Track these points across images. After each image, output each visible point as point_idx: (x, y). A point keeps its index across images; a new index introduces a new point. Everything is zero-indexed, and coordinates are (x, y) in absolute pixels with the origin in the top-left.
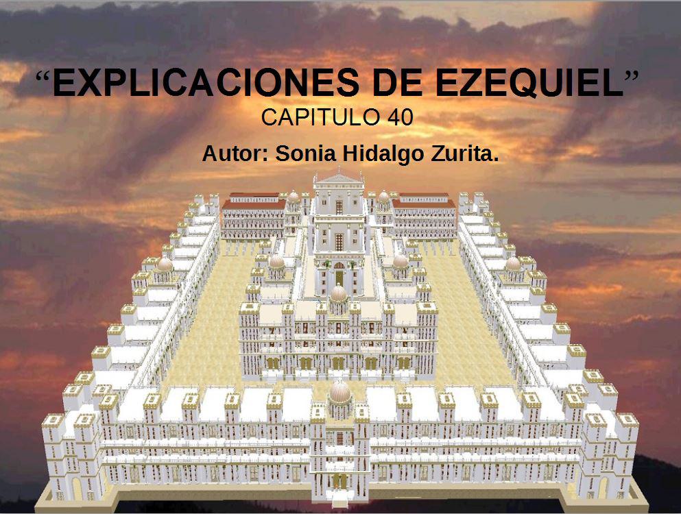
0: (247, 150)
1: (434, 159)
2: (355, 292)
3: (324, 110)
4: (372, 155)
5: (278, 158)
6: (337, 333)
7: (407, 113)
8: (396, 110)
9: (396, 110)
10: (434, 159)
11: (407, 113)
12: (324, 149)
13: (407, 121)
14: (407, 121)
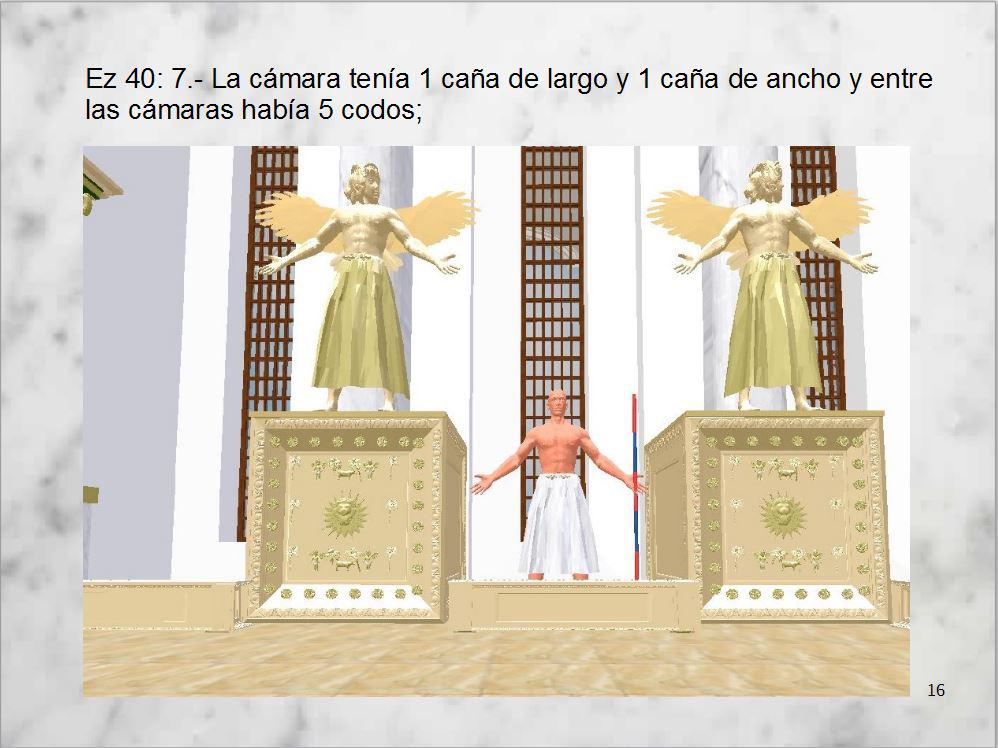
0: (512, 86)
1: (114, 75)
3: (89, 78)
4: (378, 111)
7: (148, 73)
8: (136, 70)
9: (136, 70)
10: (114, 75)
11: (148, 73)
13: (148, 83)
14: (148, 83)
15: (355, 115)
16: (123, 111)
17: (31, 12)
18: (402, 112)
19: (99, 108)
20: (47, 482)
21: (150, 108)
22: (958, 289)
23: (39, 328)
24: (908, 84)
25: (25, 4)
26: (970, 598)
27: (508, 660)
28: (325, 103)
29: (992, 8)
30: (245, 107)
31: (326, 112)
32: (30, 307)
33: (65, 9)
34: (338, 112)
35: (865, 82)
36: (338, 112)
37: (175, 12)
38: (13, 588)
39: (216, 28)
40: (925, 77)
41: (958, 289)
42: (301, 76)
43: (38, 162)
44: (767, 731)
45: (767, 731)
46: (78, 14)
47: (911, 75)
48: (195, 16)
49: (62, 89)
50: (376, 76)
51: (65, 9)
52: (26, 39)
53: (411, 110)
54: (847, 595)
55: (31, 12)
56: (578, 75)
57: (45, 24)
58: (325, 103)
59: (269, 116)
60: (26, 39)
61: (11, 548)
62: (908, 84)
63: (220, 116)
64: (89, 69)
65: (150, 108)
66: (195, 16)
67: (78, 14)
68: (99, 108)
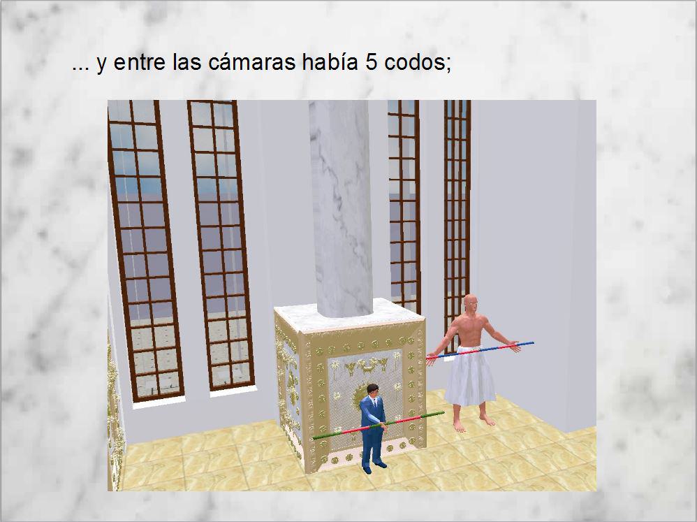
2: (43, 234)
5: (199, 60)
6: (469, 102)
12: (346, 57)
15: (396, 67)
16: (204, 62)
17: (22, 8)
18: (434, 64)
19: (184, 61)
20: (33, 336)
21: (226, 61)
22: (670, 201)
23: (28, 229)
24: (146, 66)
25: (17, 2)
26: (678, 417)
27: (174, 460)
28: (371, 57)
29: (694, 4)
30: (305, 60)
31: (372, 64)
32: (22, 214)
33: (47, 5)
34: (381, 64)
35: (110, 65)
36: (381, 64)
37: (123, 8)
38: (9, 410)
39: (152, 18)
40: (158, 61)
41: (670, 201)
42: (314, 60)
43: (27, 113)
44: (536, 510)
45: (536, 510)
46: (55, 9)
47: (149, 60)
48: (136, 11)
49: (43, 62)
50: (130, 59)
51: (47, 5)
52: (19, 26)
53: (442, 62)
54: (403, 446)
55: (22, 8)
56: (155, 59)
57: (32, 16)
58: (371, 57)
59: (323, 68)
60: (19, 26)
61: (8, 382)
62: (146, 66)
63: (189, 67)
64: (369, 54)
65: (226, 61)
66: (136, 11)
67: (55, 9)
68: (184, 61)
